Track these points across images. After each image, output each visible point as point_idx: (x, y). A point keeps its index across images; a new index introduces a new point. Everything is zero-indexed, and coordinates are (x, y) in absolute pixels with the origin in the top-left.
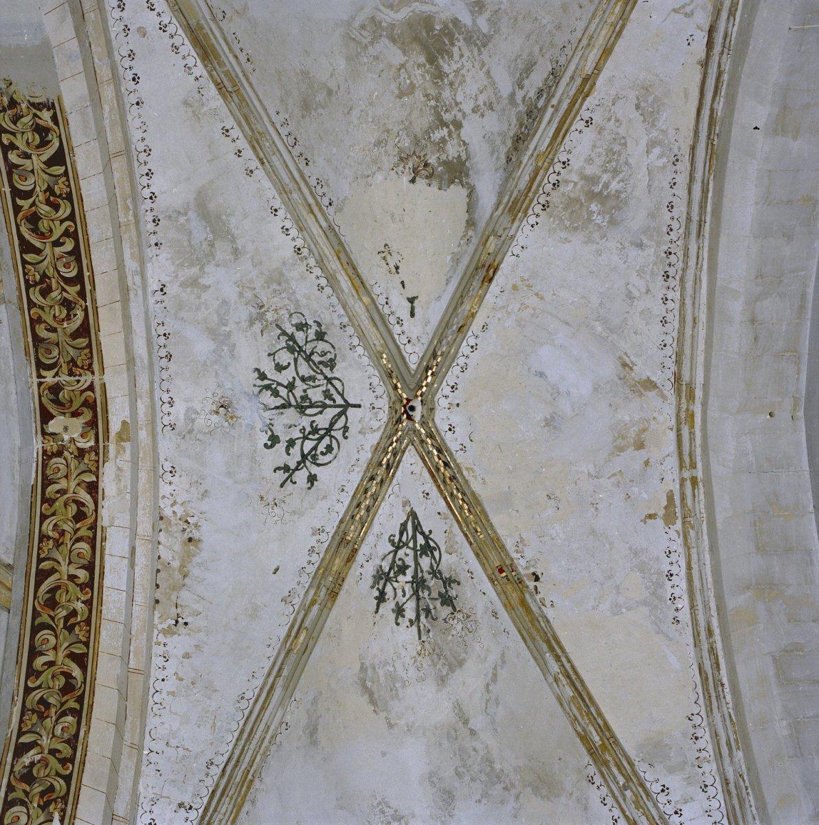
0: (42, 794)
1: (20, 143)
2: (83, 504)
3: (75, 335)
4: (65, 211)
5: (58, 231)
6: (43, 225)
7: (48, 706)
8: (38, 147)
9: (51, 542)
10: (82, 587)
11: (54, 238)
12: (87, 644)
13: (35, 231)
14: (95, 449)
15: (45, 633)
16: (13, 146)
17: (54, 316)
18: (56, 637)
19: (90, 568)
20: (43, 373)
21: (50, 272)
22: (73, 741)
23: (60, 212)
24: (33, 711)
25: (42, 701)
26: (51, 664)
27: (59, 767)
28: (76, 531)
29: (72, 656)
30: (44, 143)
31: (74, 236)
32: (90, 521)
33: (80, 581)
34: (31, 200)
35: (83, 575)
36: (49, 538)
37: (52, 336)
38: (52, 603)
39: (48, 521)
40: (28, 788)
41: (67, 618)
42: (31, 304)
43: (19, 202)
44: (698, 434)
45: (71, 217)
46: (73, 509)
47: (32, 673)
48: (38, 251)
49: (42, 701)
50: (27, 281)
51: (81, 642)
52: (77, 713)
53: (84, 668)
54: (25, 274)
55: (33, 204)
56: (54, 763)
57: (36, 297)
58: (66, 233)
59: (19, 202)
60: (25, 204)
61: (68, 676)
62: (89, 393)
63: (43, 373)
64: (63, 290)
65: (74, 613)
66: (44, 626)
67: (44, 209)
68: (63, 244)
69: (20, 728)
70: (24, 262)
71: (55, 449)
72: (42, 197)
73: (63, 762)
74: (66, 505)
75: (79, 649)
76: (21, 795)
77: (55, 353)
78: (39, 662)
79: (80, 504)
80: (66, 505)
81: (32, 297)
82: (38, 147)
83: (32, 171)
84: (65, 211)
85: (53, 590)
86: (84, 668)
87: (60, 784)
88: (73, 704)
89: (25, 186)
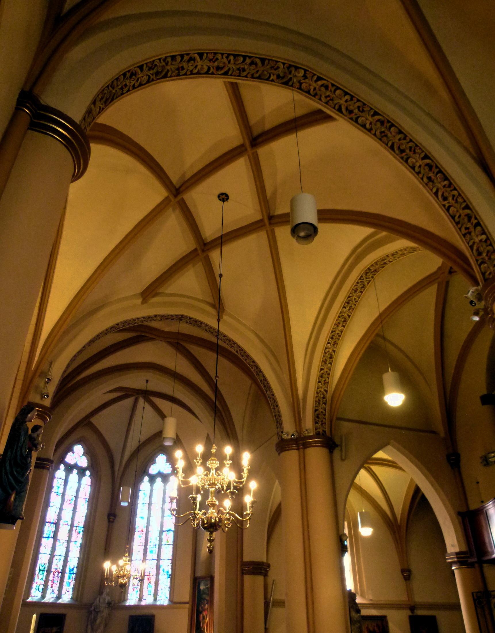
0: (410, 150)
1: (191, 68)
2: (323, 84)
3: (263, 64)
4: (219, 56)
5: (225, 60)
6: (221, 65)
7: (384, 132)
8: (195, 62)
9: (330, 102)
10: (351, 99)
11: (227, 62)
12: (371, 109)
13: (222, 68)
14: (305, 71)
15: (452, 209)
16: (191, 71)
17: (254, 69)
18: (363, 117)
19: (346, 93)
20: (271, 79)
21: (238, 67)
22: (400, 132)
23: (219, 58)
24: (383, 137)
25: (381, 132)
26: (371, 124)
27: (405, 141)
28: (331, 91)
29: (373, 116)
30: (194, 59)
31: (229, 55)
32: (330, 86)
33: (349, 100)
34: (211, 68)
35: (347, 97)
36: (328, 101)
37: (260, 72)
38: (351, 112)
39: (322, 99)
40: (405, 154)
41: (359, 110)
42: (246, 76)
43: (210, 72)
44: (488, 617)
45: (222, 54)
46: (323, 89)
47: (370, 130)
48: (229, 69)
49: (381, 132)
50: (238, 76)
51: (370, 110)
52: (392, 125)
53: (378, 114)
54: (235, 76)
55: (213, 67)
56: (404, 142)
57: (245, 74)
58: (227, 57)
59: (210, 72)
60: (212, 70)
61: (378, 120)
62: (285, 65)
63: (271, 79)
64: (246, 64)
65: (359, 107)
66: (449, 207)
67: (216, 64)
68: (230, 60)
69: (385, 144)
70: (231, 75)
71: (298, 84)
72: (212, 64)
73: (405, 139)
74: (320, 90)
75: (372, 112)
76: (405, 157)
77: (266, 73)
78: (368, 126)
79: (322, 85)
80: (320, 90)
81: (243, 75)
82: (195, 62)
83: (202, 65)
84: (219, 56)
85: (347, 109)
86: (378, 114)
87: (411, 144)
88: (388, 125)
89: (206, 69)
